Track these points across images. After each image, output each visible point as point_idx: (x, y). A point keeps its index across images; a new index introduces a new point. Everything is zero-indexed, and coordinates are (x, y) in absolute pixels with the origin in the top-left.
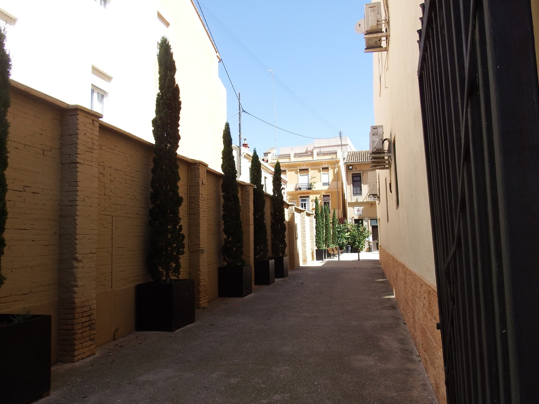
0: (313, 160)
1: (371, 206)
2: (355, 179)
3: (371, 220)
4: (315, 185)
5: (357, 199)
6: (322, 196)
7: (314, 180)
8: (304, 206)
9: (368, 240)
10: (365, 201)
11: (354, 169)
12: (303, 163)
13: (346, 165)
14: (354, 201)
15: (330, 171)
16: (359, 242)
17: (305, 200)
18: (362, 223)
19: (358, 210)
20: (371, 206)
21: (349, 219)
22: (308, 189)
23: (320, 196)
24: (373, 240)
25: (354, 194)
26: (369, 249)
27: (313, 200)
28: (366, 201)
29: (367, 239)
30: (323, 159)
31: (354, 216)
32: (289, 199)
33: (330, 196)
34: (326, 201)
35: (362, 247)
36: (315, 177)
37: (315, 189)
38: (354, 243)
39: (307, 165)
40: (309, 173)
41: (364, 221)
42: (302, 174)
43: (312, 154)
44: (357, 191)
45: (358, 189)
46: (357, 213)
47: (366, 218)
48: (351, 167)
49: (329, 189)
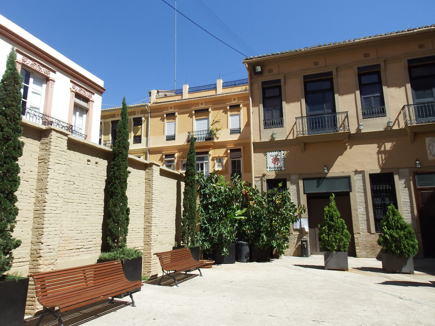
0: (216, 94)
1: (305, 149)
2: (269, 93)
3: (304, 179)
4: (218, 134)
5: (272, 136)
6: (229, 151)
7: (217, 126)
8: (200, 169)
9: (298, 227)
10: (291, 137)
11: (266, 73)
12: (200, 100)
13: (248, 63)
14: (266, 138)
15: (242, 111)
16: (271, 234)
17: (202, 159)
18: (284, 187)
19: (276, 160)
20: (305, 149)
21: (257, 179)
22: (207, 140)
23: (226, 152)
24: (310, 226)
25: (265, 124)
26: (300, 250)
27: (215, 157)
28: (292, 138)
29: (297, 225)
30: (232, 91)
31: (265, 172)
32: (178, 156)
33: (242, 150)
34: (235, 159)
35: (279, 245)
36: (219, 122)
37: (219, 140)
38: (257, 235)
39: (206, 103)
40: (210, 115)
41: (288, 183)
42: (198, 118)
43: (215, 88)
44: (273, 117)
45: (276, 113)
46: (272, 165)
47: (293, 177)
48: (259, 69)
49: (240, 138)
